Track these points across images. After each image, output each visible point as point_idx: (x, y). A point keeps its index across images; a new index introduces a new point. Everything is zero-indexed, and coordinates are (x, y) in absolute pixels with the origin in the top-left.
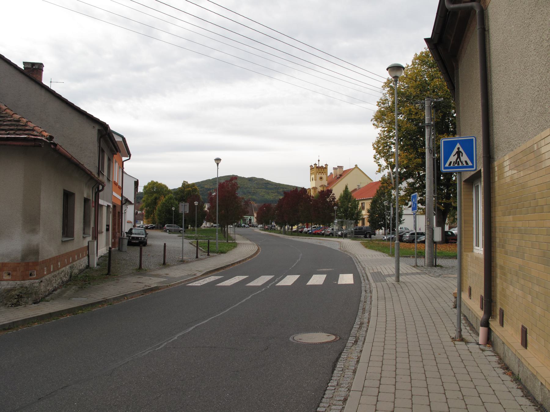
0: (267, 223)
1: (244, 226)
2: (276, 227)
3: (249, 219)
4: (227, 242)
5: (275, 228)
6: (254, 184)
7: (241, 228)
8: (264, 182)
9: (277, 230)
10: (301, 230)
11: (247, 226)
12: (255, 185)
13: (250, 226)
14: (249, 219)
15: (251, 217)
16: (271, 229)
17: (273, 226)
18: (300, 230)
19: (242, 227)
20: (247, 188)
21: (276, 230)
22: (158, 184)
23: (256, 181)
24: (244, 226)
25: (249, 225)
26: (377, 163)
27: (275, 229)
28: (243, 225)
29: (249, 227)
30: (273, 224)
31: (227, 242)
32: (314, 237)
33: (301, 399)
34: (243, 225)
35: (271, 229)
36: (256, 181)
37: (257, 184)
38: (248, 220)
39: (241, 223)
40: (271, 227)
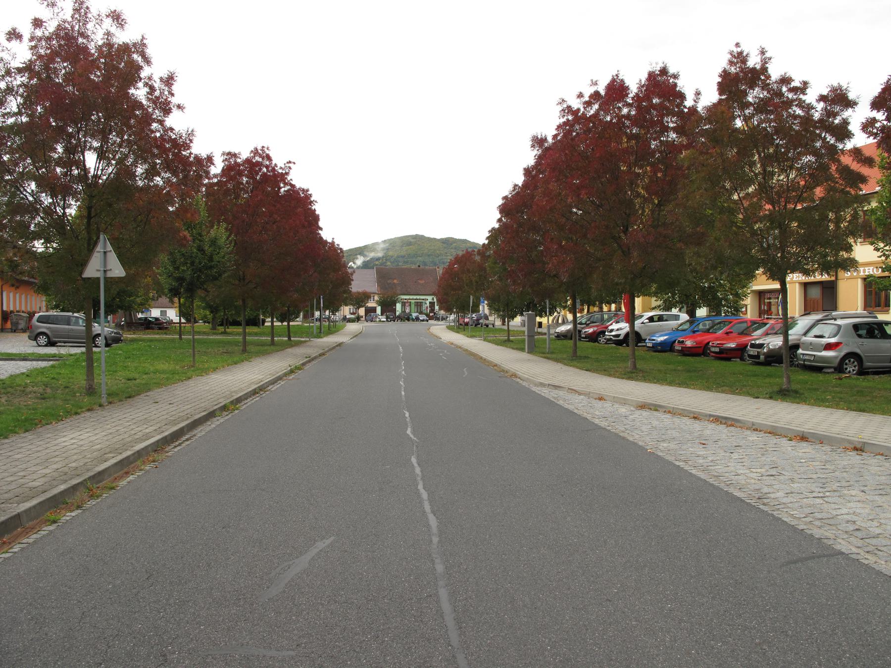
0: (463, 307)
1: (417, 319)
2: (491, 318)
3: (430, 303)
4: (181, 338)
5: (487, 322)
6: (452, 248)
7: (411, 322)
8: (468, 244)
9: (496, 330)
10: (594, 332)
11: (422, 317)
12: (452, 250)
13: (431, 318)
14: (430, 303)
15: (433, 299)
16: (476, 325)
17: (481, 318)
18: (591, 330)
19: (413, 320)
20: (439, 255)
21: (490, 326)
22: (783, 347)
23: (455, 244)
24: (417, 319)
25: (427, 315)
26: (695, 101)
27: (487, 326)
28: (414, 315)
29: (427, 321)
30: (484, 308)
31: (181, 338)
32: (820, 402)
33: (819, 192)
34: (414, 315)
35: (476, 325)
36: (455, 244)
37: (455, 248)
38: (428, 304)
39: (413, 310)
40: (478, 320)
